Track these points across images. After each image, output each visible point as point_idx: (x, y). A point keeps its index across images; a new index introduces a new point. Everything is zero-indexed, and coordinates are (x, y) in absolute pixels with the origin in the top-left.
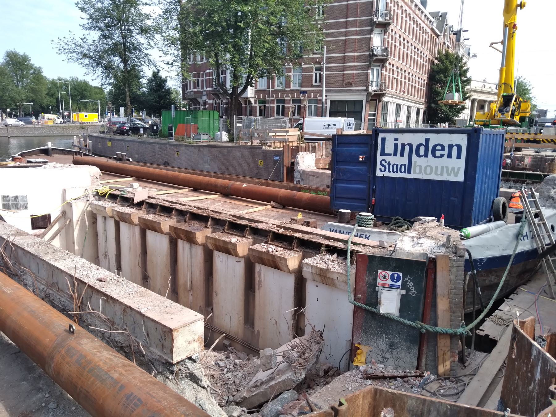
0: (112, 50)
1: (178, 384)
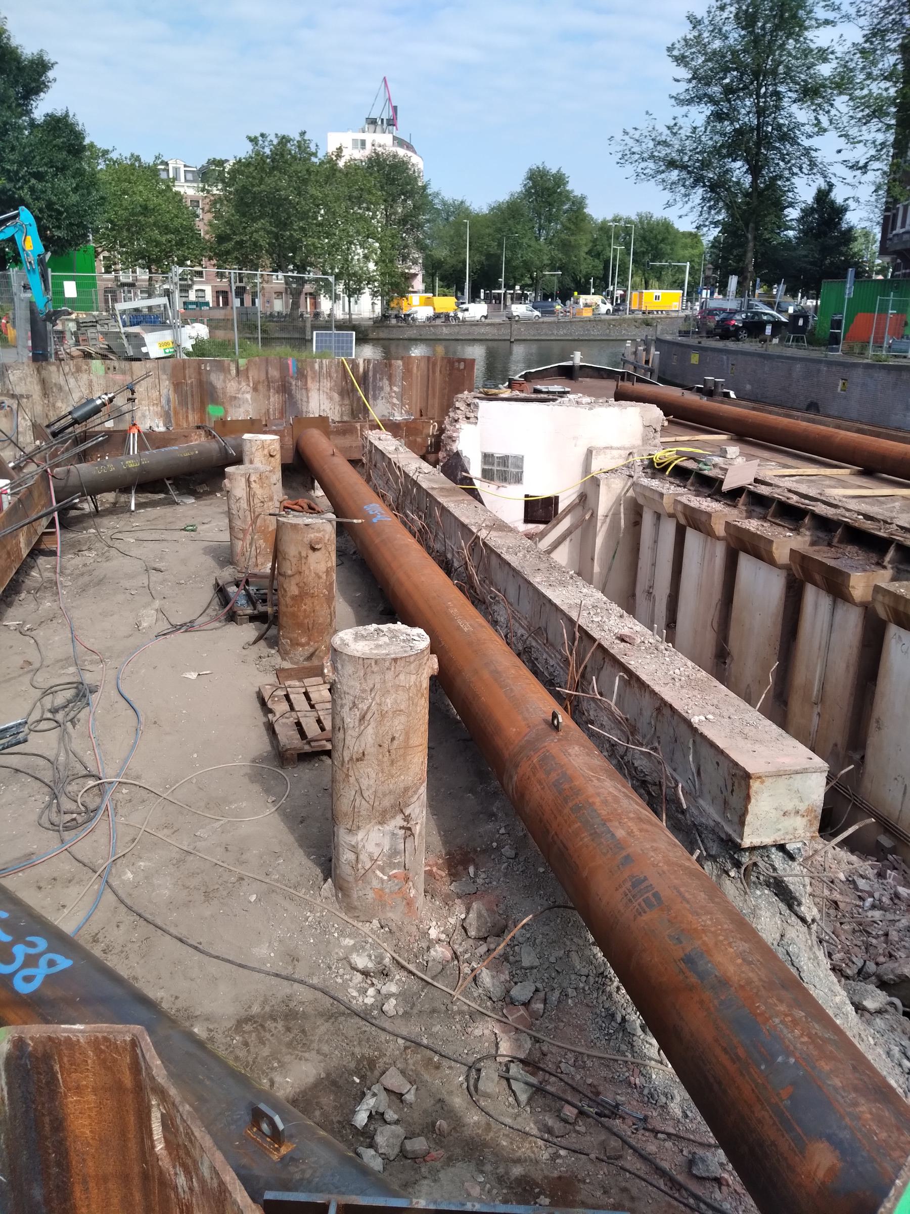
0: (730, 146)
1: (746, 893)
